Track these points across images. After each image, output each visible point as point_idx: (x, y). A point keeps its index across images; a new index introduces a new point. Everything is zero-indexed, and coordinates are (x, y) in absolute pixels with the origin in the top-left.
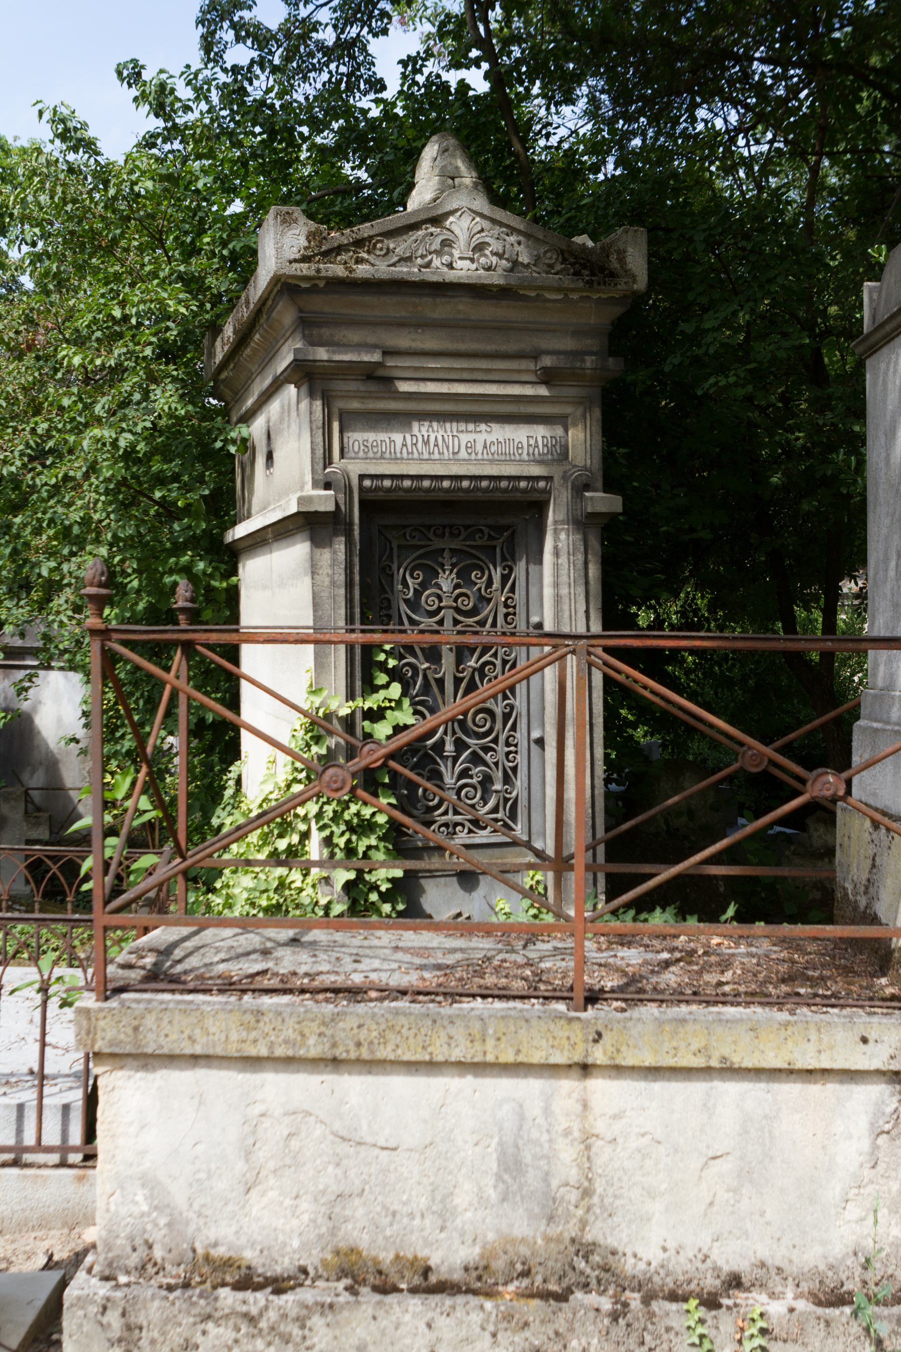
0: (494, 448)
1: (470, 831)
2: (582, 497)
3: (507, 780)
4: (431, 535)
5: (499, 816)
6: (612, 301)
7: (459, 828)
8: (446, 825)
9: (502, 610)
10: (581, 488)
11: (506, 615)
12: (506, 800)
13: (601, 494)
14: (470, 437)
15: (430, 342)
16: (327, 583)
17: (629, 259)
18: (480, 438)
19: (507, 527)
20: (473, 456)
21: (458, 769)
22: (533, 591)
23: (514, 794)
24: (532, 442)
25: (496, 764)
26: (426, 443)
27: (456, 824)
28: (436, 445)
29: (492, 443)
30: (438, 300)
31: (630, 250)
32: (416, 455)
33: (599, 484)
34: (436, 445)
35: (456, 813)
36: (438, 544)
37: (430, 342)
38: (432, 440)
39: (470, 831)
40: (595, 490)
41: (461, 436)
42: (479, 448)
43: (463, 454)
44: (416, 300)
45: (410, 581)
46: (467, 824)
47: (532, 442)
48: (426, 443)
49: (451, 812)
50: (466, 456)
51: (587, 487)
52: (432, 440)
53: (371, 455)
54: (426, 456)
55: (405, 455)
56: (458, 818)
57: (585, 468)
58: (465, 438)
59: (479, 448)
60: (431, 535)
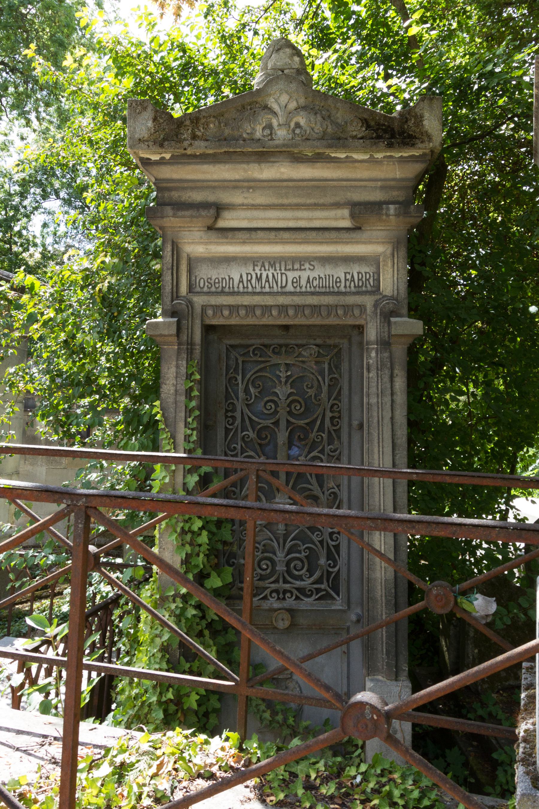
0: (316, 283)
1: (297, 598)
2: (389, 323)
3: (330, 556)
4: (270, 353)
5: (323, 586)
6: (413, 159)
7: (288, 595)
8: (277, 591)
9: (329, 414)
10: (387, 316)
11: (332, 418)
12: (329, 573)
13: (407, 319)
14: (296, 274)
15: (260, 199)
16: (172, 391)
17: (426, 123)
18: (304, 275)
19: (335, 346)
20: (298, 289)
21: (288, 545)
22: (356, 399)
23: (336, 569)
24: (349, 277)
25: (321, 542)
26: (259, 279)
27: (285, 592)
28: (267, 281)
29: (315, 278)
30: (263, 165)
31: (427, 115)
32: (250, 289)
33: (405, 311)
34: (267, 281)
35: (285, 581)
36: (275, 360)
37: (260, 199)
38: (264, 277)
39: (297, 598)
40: (401, 316)
41: (288, 273)
42: (303, 282)
43: (290, 288)
44: (245, 166)
45: (252, 390)
46: (295, 592)
47: (349, 277)
48: (259, 279)
49: (281, 580)
50: (292, 289)
51: (394, 313)
52: (264, 277)
53: (213, 289)
54: (258, 290)
55: (241, 289)
56: (287, 586)
57: (392, 298)
58: (291, 275)
59: (303, 282)
60: (270, 353)
